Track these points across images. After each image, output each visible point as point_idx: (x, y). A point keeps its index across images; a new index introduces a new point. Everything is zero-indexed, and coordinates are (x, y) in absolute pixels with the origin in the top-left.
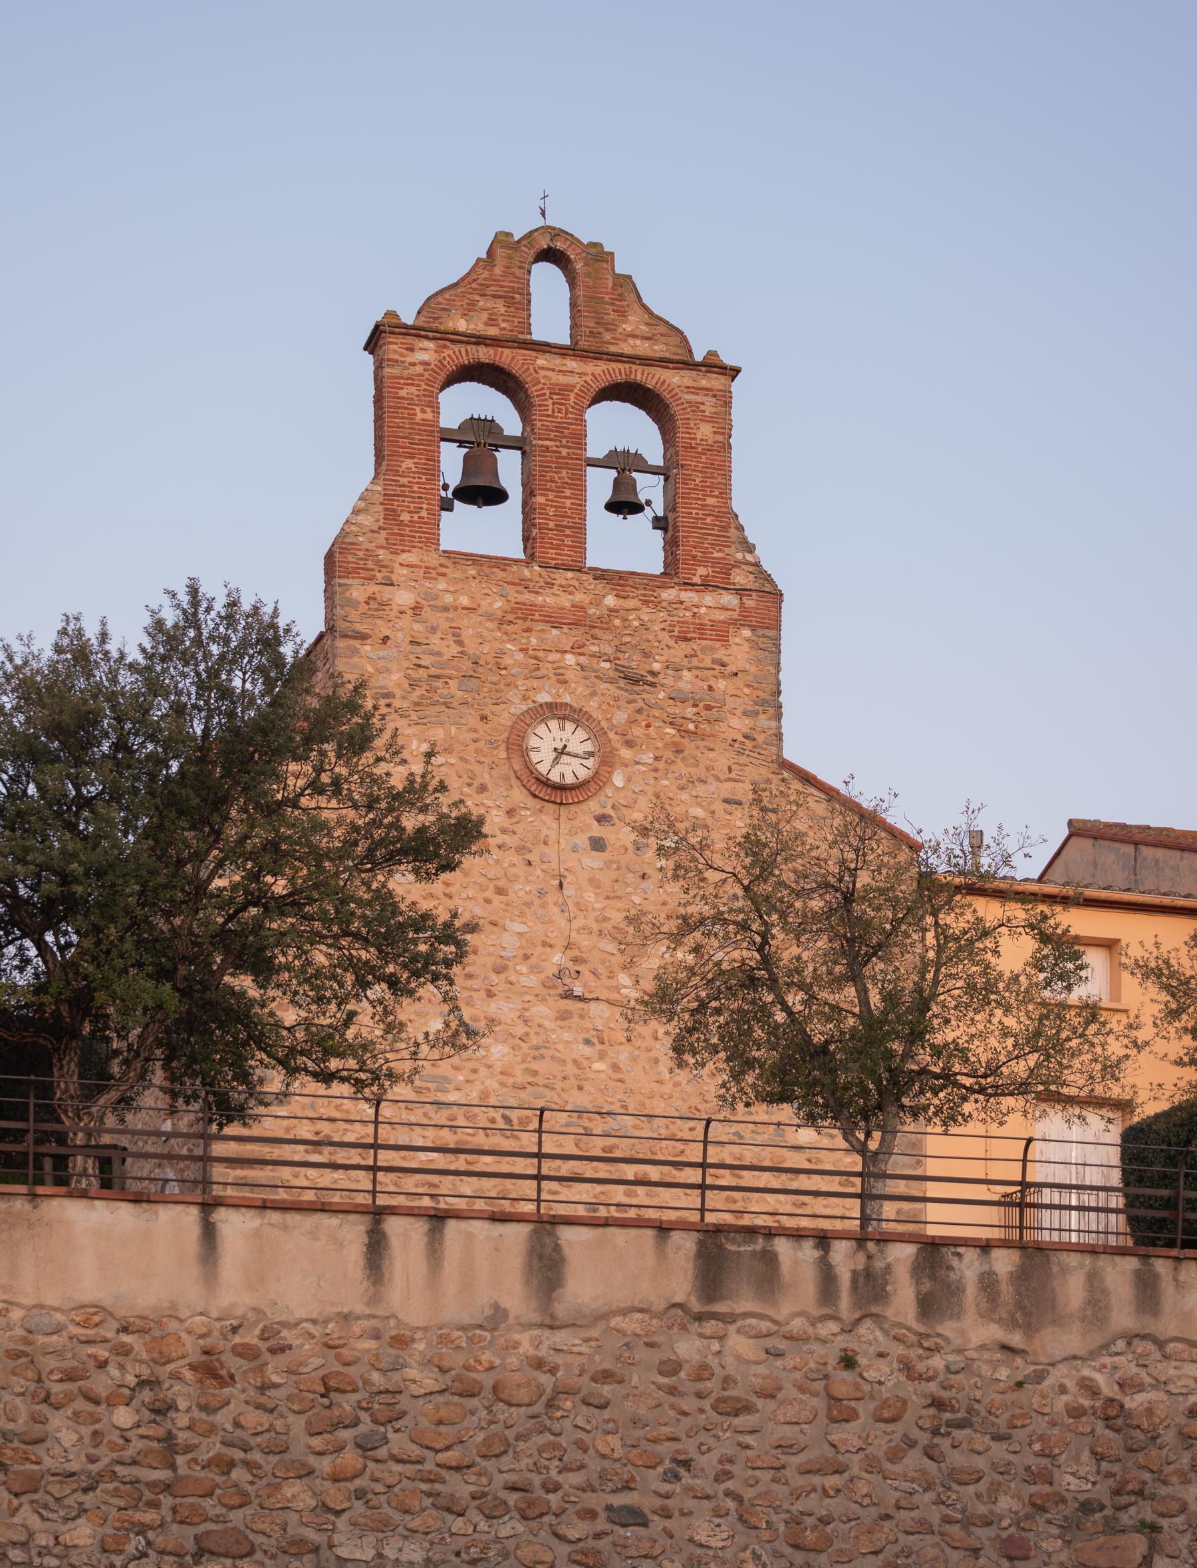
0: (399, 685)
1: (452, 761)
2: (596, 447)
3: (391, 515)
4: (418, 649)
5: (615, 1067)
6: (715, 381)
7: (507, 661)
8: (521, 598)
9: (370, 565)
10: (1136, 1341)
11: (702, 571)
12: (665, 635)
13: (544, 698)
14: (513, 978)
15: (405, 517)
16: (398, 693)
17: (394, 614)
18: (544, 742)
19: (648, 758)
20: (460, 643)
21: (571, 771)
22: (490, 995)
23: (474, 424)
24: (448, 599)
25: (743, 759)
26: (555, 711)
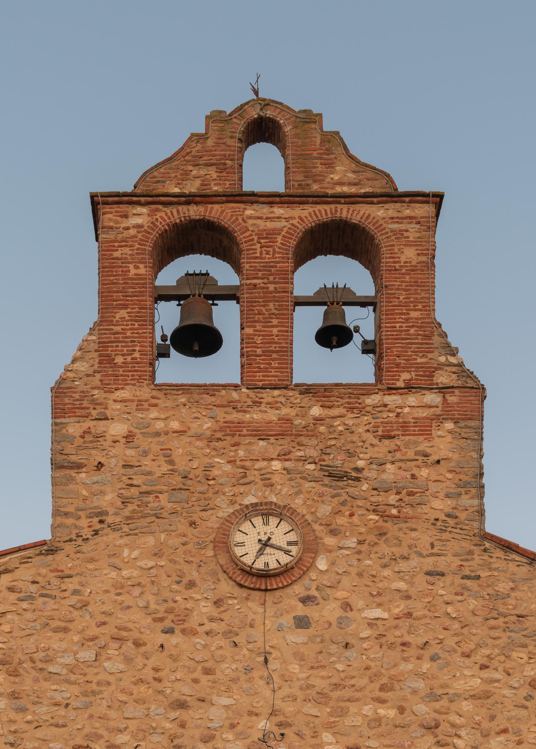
3: (106, 360)
7: (216, 472)
9: (85, 404)
11: (405, 376)
20: (171, 462)
24: (160, 425)
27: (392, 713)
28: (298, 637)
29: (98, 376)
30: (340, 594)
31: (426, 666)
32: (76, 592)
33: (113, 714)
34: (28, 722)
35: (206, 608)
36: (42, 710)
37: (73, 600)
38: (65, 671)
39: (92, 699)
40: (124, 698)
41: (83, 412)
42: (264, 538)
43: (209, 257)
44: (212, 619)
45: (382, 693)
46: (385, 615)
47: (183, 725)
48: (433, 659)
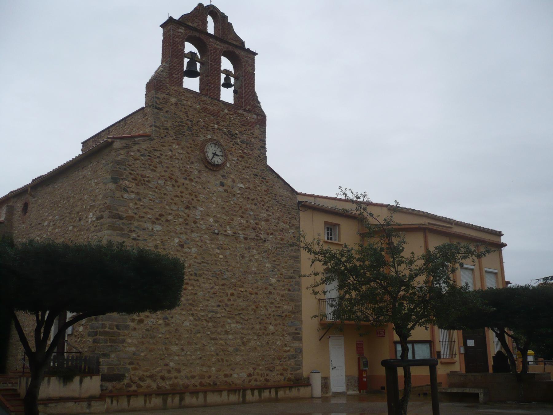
0: (170, 126)
1: (184, 153)
2: (186, 51)
3: (171, 74)
4: (176, 116)
5: (225, 257)
6: (251, 56)
7: (200, 124)
8: (204, 106)
9: (164, 88)
10: (93, 403)
11: (248, 107)
12: (239, 123)
13: (209, 137)
14: (199, 226)
15: (174, 76)
16: (170, 128)
17: (170, 104)
18: (211, 150)
19: (235, 159)
20: (188, 116)
21: (218, 160)
22: (192, 231)
23: (191, 53)
24: (185, 102)
25: (258, 163)
26: (217, 143)
27: (245, 222)
28: (221, 189)
29: (168, 79)
30: (232, 176)
31: (253, 206)
32: (159, 157)
33: (167, 207)
34: (141, 205)
35: (196, 172)
36: (146, 201)
37: (158, 160)
38: (154, 187)
39: (278, 309)
40: (172, 201)
41: (163, 91)
42: (214, 152)
43: (162, 38)
44: (198, 177)
45: (476, 392)
46: (243, 187)
47: (188, 216)
48: (255, 204)
